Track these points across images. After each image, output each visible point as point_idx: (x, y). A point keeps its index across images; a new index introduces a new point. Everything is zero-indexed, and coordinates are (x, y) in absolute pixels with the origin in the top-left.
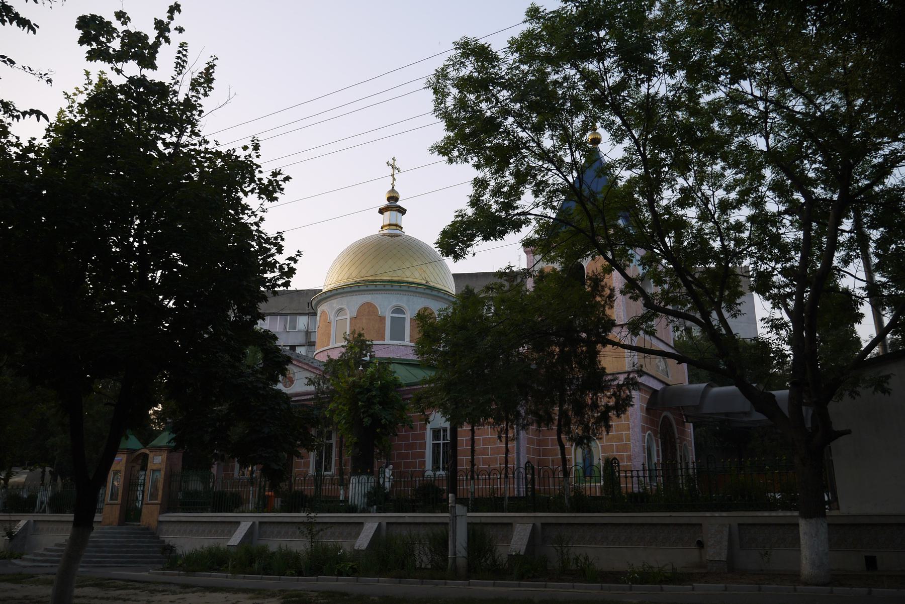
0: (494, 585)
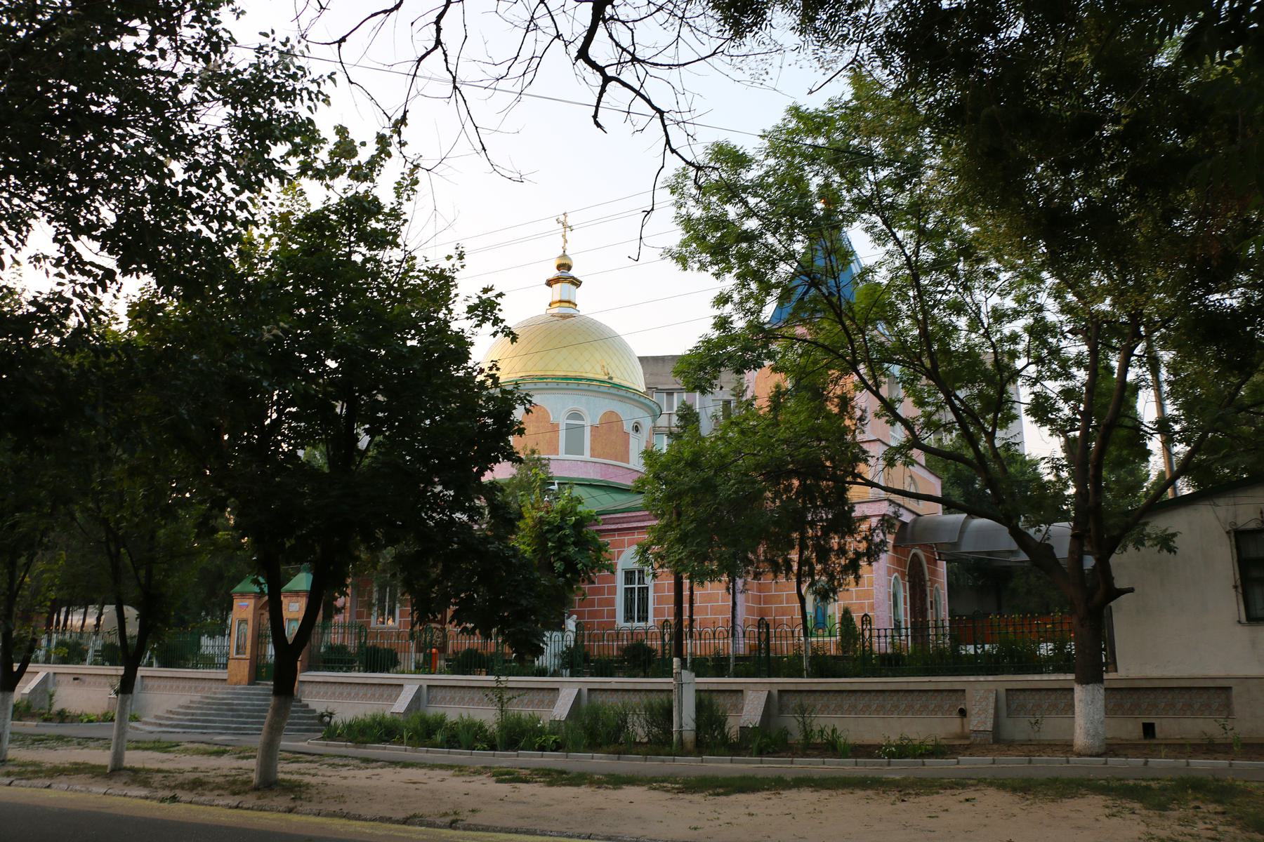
0: (732, 761)
